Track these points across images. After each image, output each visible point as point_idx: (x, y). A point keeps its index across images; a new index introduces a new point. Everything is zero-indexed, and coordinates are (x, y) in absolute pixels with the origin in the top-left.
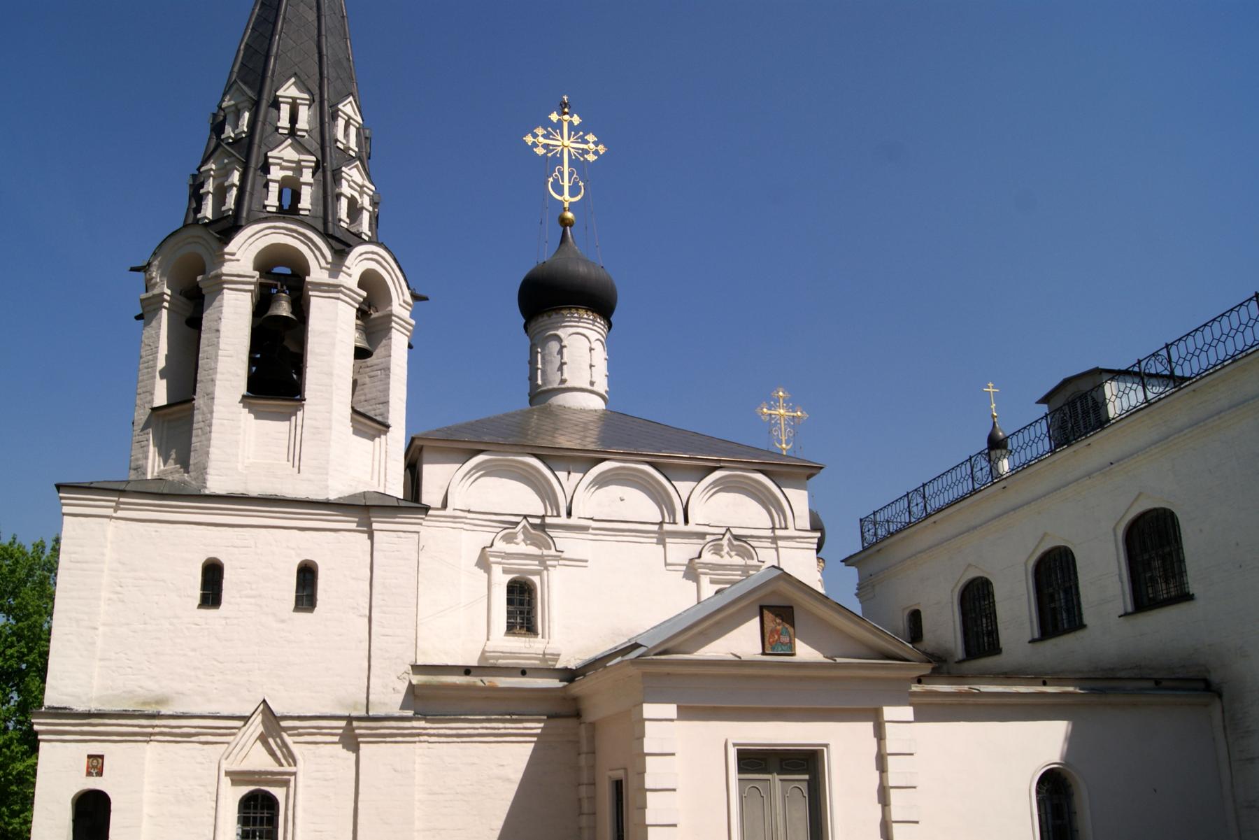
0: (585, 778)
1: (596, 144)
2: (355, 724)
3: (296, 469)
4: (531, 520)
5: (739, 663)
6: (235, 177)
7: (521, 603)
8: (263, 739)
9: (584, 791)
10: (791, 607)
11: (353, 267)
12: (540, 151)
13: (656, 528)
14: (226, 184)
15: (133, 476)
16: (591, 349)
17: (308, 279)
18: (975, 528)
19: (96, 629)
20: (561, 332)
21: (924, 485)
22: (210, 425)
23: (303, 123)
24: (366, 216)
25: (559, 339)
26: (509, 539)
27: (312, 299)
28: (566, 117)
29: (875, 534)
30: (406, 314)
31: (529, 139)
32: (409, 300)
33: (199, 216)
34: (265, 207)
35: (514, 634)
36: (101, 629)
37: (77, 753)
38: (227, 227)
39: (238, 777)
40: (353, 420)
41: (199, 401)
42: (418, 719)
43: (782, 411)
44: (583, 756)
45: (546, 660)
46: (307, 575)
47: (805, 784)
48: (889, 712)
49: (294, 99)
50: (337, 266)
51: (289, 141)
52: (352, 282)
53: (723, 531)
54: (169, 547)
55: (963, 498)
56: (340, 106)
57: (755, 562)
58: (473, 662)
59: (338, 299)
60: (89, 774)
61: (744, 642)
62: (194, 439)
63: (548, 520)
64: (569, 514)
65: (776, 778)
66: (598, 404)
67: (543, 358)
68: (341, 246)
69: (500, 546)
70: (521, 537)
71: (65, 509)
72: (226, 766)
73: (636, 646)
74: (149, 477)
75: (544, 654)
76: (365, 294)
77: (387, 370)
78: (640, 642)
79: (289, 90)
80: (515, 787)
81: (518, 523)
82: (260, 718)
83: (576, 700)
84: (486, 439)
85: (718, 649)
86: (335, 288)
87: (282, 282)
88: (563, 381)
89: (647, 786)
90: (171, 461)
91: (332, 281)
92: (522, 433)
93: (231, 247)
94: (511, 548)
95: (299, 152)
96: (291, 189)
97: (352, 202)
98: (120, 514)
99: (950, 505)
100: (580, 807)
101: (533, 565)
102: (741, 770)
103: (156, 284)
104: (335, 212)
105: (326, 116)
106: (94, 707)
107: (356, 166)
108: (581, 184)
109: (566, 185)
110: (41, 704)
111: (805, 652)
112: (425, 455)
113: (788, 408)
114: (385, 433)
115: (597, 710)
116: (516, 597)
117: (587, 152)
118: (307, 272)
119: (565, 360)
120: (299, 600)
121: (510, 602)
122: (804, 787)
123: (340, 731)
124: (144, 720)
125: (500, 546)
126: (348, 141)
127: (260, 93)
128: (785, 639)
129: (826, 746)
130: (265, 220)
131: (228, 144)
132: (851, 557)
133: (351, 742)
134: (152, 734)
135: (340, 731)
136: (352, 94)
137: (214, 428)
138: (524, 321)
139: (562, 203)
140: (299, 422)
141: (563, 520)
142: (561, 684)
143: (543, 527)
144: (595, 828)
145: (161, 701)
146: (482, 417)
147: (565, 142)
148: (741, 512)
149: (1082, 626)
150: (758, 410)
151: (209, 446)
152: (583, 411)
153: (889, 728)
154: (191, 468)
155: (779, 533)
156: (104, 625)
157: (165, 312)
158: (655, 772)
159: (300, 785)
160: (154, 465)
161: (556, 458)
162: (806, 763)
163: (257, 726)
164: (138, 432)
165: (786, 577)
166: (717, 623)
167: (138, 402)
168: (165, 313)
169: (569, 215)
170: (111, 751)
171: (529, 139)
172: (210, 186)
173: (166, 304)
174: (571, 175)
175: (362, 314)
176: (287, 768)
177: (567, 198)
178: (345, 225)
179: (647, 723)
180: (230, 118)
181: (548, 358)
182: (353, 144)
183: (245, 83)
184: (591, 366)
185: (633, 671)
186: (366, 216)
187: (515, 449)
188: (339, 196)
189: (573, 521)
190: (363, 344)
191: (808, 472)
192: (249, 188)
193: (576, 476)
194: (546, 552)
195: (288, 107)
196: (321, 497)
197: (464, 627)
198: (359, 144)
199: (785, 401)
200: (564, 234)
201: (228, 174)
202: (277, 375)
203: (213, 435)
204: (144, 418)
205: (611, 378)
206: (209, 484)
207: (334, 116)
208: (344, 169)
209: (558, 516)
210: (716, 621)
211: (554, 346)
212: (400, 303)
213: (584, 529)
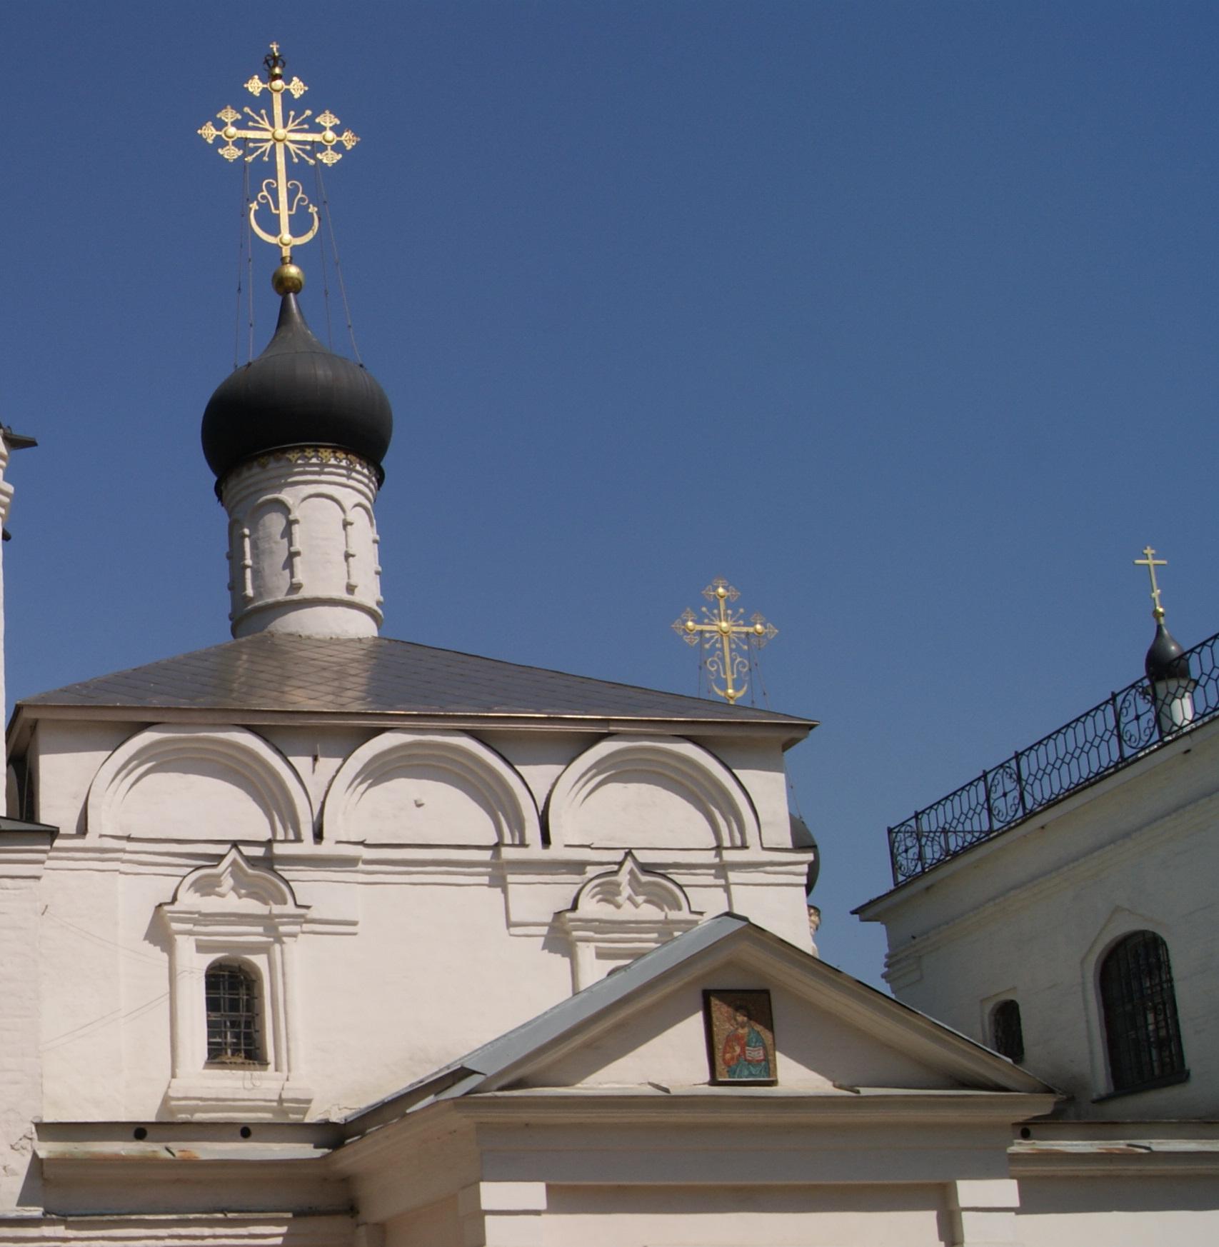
1: (338, 130)
4: (247, 851)
5: (666, 1101)
7: (234, 1005)
10: (766, 993)
12: (231, 153)
13: (486, 856)
16: (346, 524)
18: (1127, 835)
20: (286, 496)
21: (1018, 756)
25: (283, 508)
26: (206, 887)
28: (278, 84)
29: (921, 857)
31: (209, 132)
35: (223, 1065)
42: (52, 1223)
43: (724, 625)
45: (285, 1112)
48: (969, 1191)
53: (619, 856)
55: (1100, 777)
57: (684, 914)
58: (148, 1114)
61: (674, 1059)
63: (279, 849)
64: (318, 836)
66: (364, 628)
67: (254, 546)
69: (190, 900)
70: (228, 882)
73: (462, 1073)
75: (281, 1101)
78: (468, 1065)
81: (221, 857)
83: (346, 1181)
84: (156, 702)
85: (624, 1075)
88: (295, 588)
92: (224, 687)
99: (1089, 783)
101: (254, 934)
108: (313, 209)
109: (284, 214)
111: (794, 1077)
112: (43, 737)
113: (735, 618)
116: (224, 995)
119: (297, 546)
121: (212, 1005)
125: (190, 900)
128: (756, 1054)
132: (871, 903)
138: (213, 479)
139: (277, 248)
141: (307, 847)
142: (319, 1153)
143: (268, 862)
147: (279, 132)
148: (656, 819)
149: (145, 939)
150: (677, 624)
152: (335, 642)
153: (969, 1221)
155: (729, 856)
161: (288, 731)
165: (753, 932)
166: (620, 1026)
169: (293, 270)
171: (209, 132)
174: (291, 194)
179: (488, 1219)
181: (263, 545)
184: (348, 556)
185: (461, 1120)
193: (328, 764)
194: (277, 909)
199: (729, 604)
200: (285, 307)
205: (387, 577)
209: (298, 839)
210: (621, 1021)
211: (275, 522)
213: (349, 862)
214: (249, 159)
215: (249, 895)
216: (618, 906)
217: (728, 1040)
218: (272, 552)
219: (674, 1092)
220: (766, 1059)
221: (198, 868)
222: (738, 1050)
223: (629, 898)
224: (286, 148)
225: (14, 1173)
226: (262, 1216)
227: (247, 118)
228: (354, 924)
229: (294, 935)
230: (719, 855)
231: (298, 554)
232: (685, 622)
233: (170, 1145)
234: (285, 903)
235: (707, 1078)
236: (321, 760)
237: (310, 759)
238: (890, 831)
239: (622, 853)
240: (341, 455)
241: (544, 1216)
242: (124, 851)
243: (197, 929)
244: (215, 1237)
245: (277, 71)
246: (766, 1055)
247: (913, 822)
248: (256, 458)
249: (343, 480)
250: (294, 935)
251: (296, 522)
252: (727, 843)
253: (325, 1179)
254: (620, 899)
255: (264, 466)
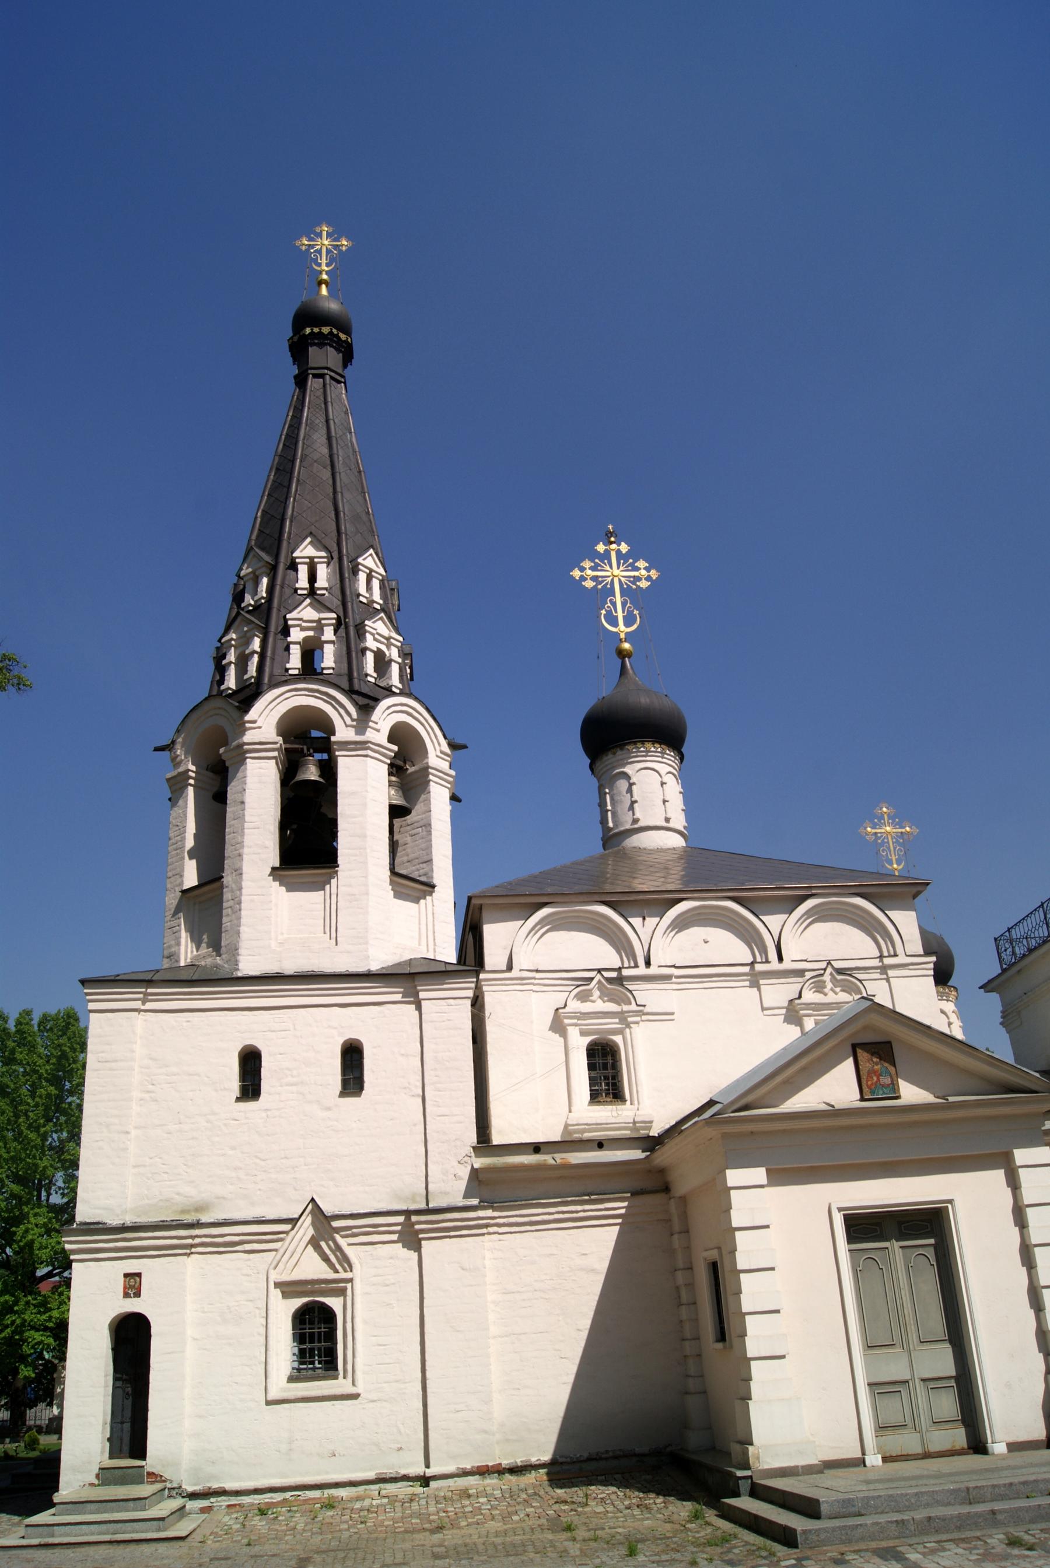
0: (680, 1264)
1: (647, 569)
2: (414, 1218)
3: (333, 941)
4: (606, 974)
5: (833, 1113)
6: (256, 644)
7: (605, 1067)
8: (314, 1243)
9: (681, 1277)
10: (889, 1043)
11: (380, 722)
12: (589, 584)
13: (747, 969)
14: (247, 652)
15: (166, 964)
17: (333, 739)
19: (128, 1133)
20: (628, 769)
22: (240, 903)
23: (322, 582)
24: (395, 669)
25: (627, 777)
26: (584, 997)
27: (339, 759)
28: (614, 546)
30: (445, 765)
31: (576, 573)
32: (447, 750)
33: (223, 687)
34: (287, 670)
35: (599, 1103)
36: (134, 1133)
37: (113, 1272)
38: (248, 695)
39: (289, 1289)
40: (392, 882)
41: (228, 879)
42: (484, 1208)
43: (888, 829)
44: (676, 1237)
45: (638, 1130)
46: (352, 1056)
47: (932, 1249)
48: (1022, 1156)
49: (311, 558)
50: (362, 723)
51: (308, 601)
52: (382, 738)
53: (823, 965)
54: (203, 1036)
56: (360, 560)
59: (366, 756)
60: (126, 1295)
61: (838, 1087)
62: (224, 920)
63: (625, 972)
64: (648, 963)
65: (895, 1246)
66: (678, 842)
67: (612, 799)
68: (366, 702)
69: (575, 1006)
70: (596, 993)
71: (91, 1006)
72: (275, 1276)
73: (711, 1103)
74: (182, 964)
75: (634, 1123)
76: (395, 748)
77: (427, 826)
79: (306, 550)
80: (601, 1278)
81: (592, 979)
82: (309, 1219)
83: (662, 1171)
84: (549, 890)
85: (808, 1099)
86: (363, 745)
87: (307, 743)
88: (636, 821)
89: (740, 1267)
90: (204, 945)
91: (359, 738)
92: (601, 883)
93: (252, 715)
94: (587, 1007)
95: (319, 611)
96: (310, 652)
97: (379, 655)
98: (149, 1006)
100: (679, 1297)
101: (613, 1024)
102: (851, 1238)
103: (182, 761)
104: (361, 666)
105: (346, 571)
106: (129, 1219)
107: (381, 619)
108: (636, 612)
110: (72, 1218)
111: (911, 1093)
112: (485, 915)
113: (894, 825)
114: (431, 894)
115: (684, 1183)
116: (599, 1061)
117: (639, 579)
118: (333, 733)
120: (345, 1083)
121: (591, 1067)
122: (930, 1253)
123: (399, 1228)
124: (184, 1231)
125: (575, 1006)
126: (371, 595)
127: (277, 557)
128: (886, 1080)
129: (950, 1201)
130: (285, 683)
131: (249, 612)
132: (990, 981)
133: (411, 1240)
134: (192, 1246)
135: (399, 1228)
136: (372, 547)
137: (243, 905)
138: (587, 761)
139: (617, 634)
140: (334, 890)
141: (642, 970)
142: (643, 1155)
143: (620, 980)
144: (697, 1320)
145: (200, 1209)
146: (536, 870)
147: (615, 571)
148: (840, 942)
150: (861, 830)
151: (239, 926)
153: (1025, 1176)
154: (223, 950)
155: (887, 961)
156: (136, 1128)
157: (191, 790)
158: (747, 1250)
159: (357, 1292)
160: (187, 951)
161: (632, 903)
162: (929, 1224)
163: (306, 1229)
164: (168, 918)
166: (804, 1069)
167: (169, 886)
168: (191, 790)
169: (626, 646)
170: (151, 1269)
171: (576, 573)
172: (231, 656)
173: (192, 781)
174: (624, 604)
175: (396, 769)
176: (343, 1275)
177: (622, 629)
178: (373, 680)
180: (249, 586)
181: (616, 798)
182: (377, 596)
183: (263, 549)
185: (711, 1132)
186: (395, 669)
187: (582, 898)
188: (364, 650)
189: (653, 970)
190: (399, 801)
191: (914, 890)
192: (269, 653)
193: (651, 921)
194: (626, 1008)
195: (306, 567)
196: (361, 968)
197: (541, 1099)
198: (384, 596)
200: (623, 666)
201: (248, 642)
202: (309, 843)
203: (243, 913)
204: (175, 902)
205: (687, 812)
206: (241, 966)
207: (355, 571)
208: (367, 622)
209: (636, 966)
210: (802, 1066)
211: (622, 784)
212: (437, 754)
213: (667, 978)
214: (600, 587)
215: (608, 1001)
216: (826, 995)
217: (869, 1073)
218: (621, 802)
219: (837, 1107)
220: (892, 1083)
221: (578, 986)
222: (875, 1078)
223: (832, 989)
224: (620, 580)
225: (461, 1179)
226: (612, 1196)
227: (597, 565)
228: (673, 1014)
229: (637, 1023)
230: (881, 961)
231: (636, 802)
232: (865, 828)
233: (555, 1155)
234: (630, 1004)
235: (858, 1097)
236: (647, 919)
237: (641, 919)
238: (996, 939)
239: (825, 963)
240: (657, 745)
241: (766, 1189)
242: (534, 978)
243: (580, 1022)
244: (584, 1211)
245: (613, 539)
246: (892, 1081)
247: (1007, 934)
248: (609, 750)
249: (660, 759)
250: (637, 1023)
251: (634, 784)
252: (886, 954)
253: (650, 1171)
254: (826, 990)
255: (614, 754)
